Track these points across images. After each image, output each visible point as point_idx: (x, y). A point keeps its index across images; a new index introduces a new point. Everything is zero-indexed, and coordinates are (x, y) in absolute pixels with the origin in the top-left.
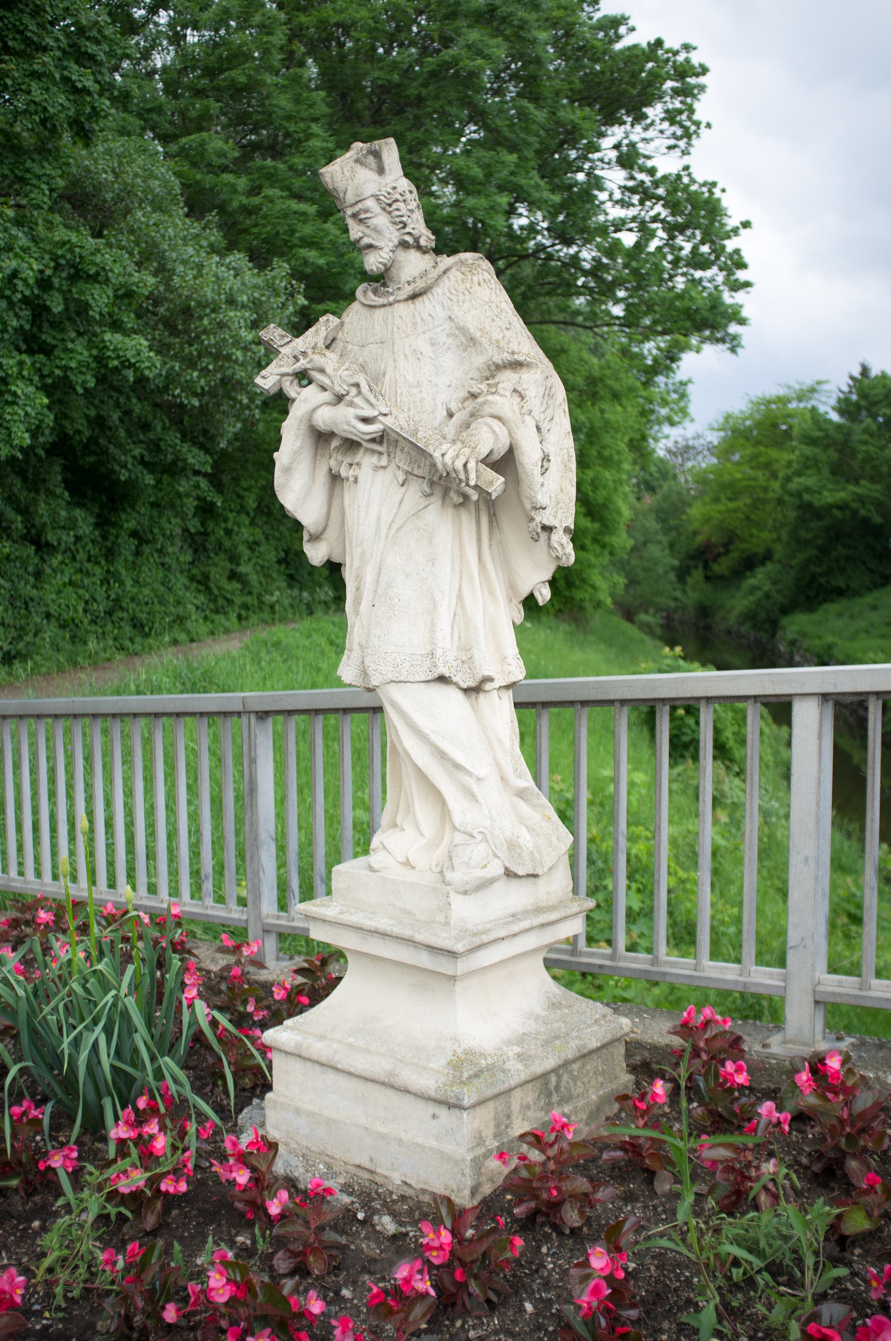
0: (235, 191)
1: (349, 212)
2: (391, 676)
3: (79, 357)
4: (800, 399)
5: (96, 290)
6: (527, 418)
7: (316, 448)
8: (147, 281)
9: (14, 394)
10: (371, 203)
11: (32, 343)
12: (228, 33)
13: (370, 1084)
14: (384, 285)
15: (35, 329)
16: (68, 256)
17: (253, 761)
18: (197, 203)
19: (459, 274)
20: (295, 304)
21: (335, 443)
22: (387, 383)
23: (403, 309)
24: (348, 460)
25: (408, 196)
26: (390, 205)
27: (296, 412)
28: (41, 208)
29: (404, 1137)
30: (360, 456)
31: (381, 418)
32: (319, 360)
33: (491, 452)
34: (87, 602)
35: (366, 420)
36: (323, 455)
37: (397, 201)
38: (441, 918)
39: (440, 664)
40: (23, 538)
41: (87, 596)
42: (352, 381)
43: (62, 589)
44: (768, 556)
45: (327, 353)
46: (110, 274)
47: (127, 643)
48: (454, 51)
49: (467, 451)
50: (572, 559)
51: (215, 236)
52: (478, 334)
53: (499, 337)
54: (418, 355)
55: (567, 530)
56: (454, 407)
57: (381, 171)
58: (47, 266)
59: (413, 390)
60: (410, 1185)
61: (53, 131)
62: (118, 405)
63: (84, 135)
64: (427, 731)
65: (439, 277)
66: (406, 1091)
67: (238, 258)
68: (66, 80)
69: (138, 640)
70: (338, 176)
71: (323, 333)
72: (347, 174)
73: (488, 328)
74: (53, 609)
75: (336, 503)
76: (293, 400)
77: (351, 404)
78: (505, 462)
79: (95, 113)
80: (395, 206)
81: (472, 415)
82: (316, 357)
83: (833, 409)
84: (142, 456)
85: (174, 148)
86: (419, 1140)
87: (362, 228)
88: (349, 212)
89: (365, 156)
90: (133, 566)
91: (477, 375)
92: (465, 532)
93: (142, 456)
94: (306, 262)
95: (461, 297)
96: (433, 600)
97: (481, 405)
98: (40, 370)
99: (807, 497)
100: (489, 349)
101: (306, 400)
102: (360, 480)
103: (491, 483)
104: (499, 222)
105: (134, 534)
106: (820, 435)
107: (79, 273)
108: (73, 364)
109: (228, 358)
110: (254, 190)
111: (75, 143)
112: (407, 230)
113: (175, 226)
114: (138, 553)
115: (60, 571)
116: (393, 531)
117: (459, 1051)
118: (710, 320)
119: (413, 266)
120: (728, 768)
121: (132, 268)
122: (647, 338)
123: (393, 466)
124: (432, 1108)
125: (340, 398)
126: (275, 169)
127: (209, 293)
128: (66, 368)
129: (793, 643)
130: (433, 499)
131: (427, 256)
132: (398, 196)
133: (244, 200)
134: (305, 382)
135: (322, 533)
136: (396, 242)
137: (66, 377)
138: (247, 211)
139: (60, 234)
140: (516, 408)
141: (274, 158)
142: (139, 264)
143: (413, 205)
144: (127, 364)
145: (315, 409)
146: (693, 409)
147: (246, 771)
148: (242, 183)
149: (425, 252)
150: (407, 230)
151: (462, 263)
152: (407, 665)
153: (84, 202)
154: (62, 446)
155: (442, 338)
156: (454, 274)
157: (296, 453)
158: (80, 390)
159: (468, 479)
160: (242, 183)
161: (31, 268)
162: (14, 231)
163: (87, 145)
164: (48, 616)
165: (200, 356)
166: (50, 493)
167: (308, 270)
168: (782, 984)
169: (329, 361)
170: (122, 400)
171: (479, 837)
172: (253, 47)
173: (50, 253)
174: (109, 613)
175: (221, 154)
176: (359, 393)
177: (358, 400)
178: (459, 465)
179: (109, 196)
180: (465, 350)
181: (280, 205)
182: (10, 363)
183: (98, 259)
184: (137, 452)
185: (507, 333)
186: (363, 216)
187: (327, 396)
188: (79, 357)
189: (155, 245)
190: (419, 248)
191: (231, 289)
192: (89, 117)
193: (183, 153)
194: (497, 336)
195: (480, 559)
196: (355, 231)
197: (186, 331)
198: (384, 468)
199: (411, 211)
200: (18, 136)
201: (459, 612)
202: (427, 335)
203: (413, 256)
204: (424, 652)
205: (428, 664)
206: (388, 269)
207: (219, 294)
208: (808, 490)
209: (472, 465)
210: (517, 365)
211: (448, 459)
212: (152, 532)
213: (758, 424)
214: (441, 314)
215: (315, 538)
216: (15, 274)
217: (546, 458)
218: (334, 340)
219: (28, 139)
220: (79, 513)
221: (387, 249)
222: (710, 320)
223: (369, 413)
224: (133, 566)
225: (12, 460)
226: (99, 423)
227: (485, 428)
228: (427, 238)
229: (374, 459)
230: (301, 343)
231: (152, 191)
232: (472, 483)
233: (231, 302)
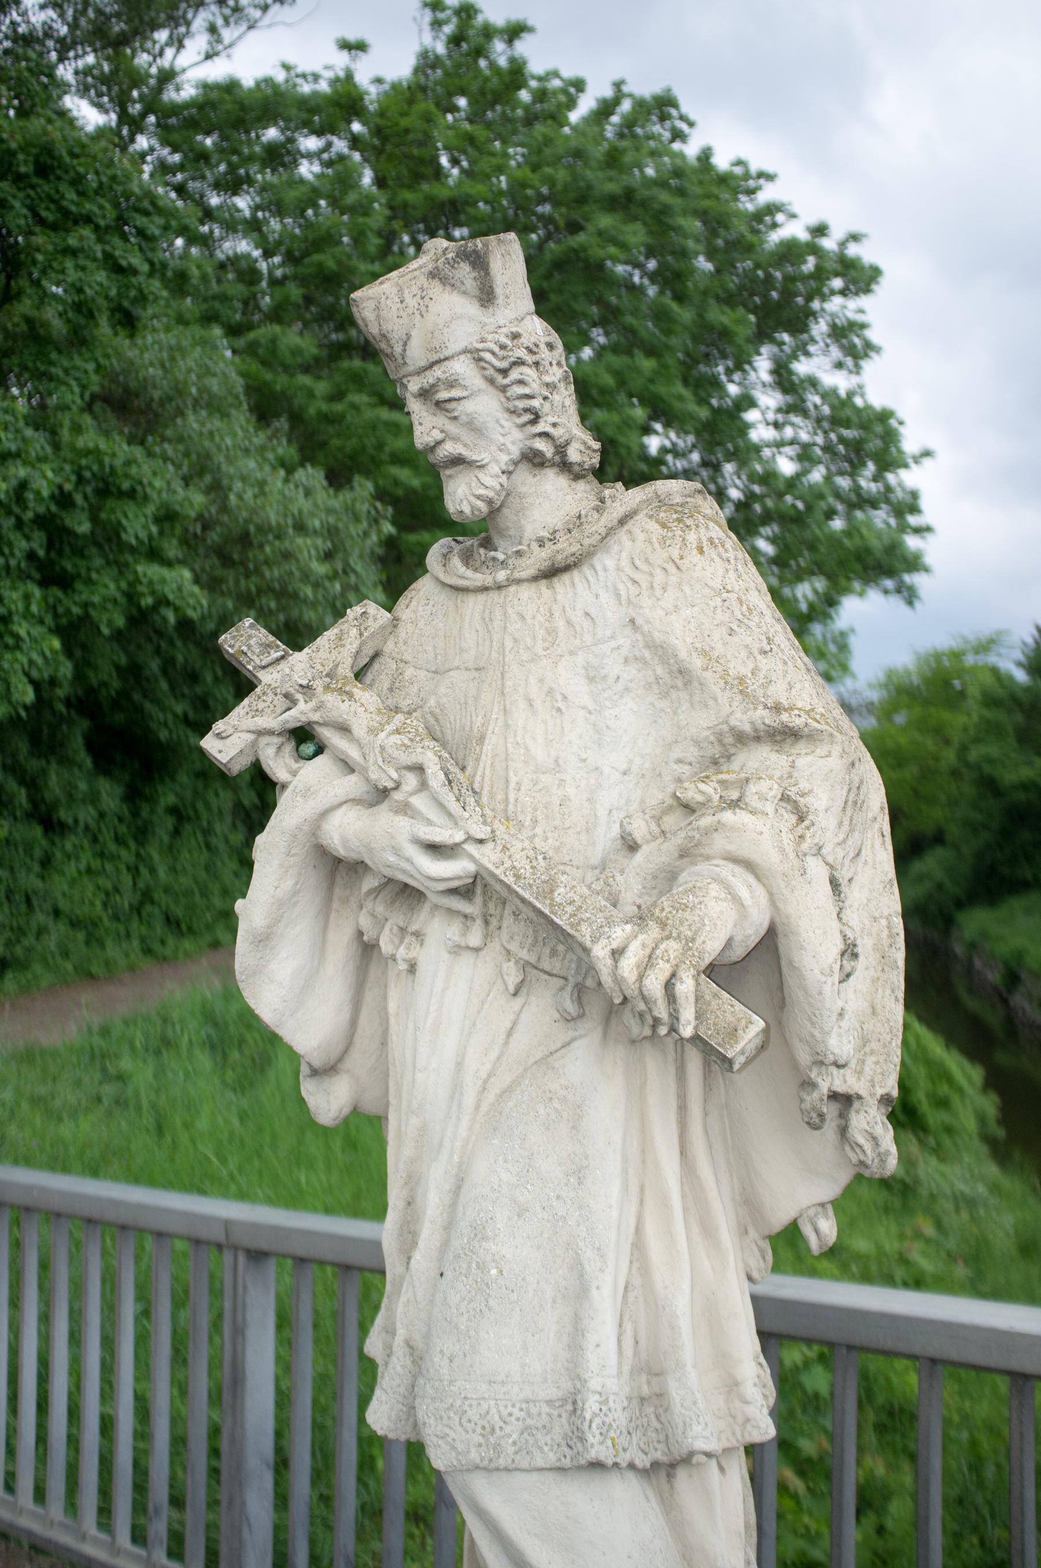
0: (311, 394)
1: (414, 385)
3: (103, 591)
4: (977, 652)
5: (131, 508)
6: (812, 862)
7: (329, 899)
8: (195, 500)
9: (17, 637)
10: (462, 367)
11: (52, 576)
12: (316, 214)
14: (487, 543)
15: (53, 555)
16: (95, 468)
17: (239, 1332)
18: (265, 406)
19: (653, 526)
20: (379, 531)
21: (369, 883)
22: (486, 759)
23: (528, 598)
24: (397, 919)
25: (545, 354)
26: (504, 372)
27: (288, 816)
28: (68, 408)
30: (425, 920)
32: (337, 706)
33: (729, 944)
34: (107, 894)
35: (434, 848)
36: (345, 901)
37: (519, 363)
39: (593, 1438)
40: (29, 815)
41: (109, 886)
42: (406, 759)
43: (75, 882)
44: (939, 838)
45: (357, 691)
46: (148, 490)
47: (156, 946)
48: (581, 238)
49: (673, 947)
50: (892, 1163)
51: (285, 449)
52: (697, 663)
53: (746, 671)
54: (557, 701)
55: (885, 1100)
56: (639, 829)
57: (487, 296)
58: (68, 480)
59: (546, 779)
61: (91, 315)
62: (158, 651)
63: (127, 321)
65: (610, 532)
67: (312, 476)
68: (108, 256)
69: (171, 941)
70: (392, 308)
71: (352, 643)
72: (412, 302)
73: (719, 649)
74: (63, 905)
75: (370, 998)
76: (284, 786)
77: (405, 809)
78: (758, 967)
79: (142, 298)
80: (514, 374)
81: (684, 853)
82: (331, 699)
83: (1019, 664)
84: (185, 715)
85: (241, 342)
87: (441, 420)
89: (452, 264)
90: (171, 850)
91: (692, 753)
92: (653, 1100)
93: (185, 715)
94: (396, 482)
95: (659, 577)
96: (578, 1268)
97: (707, 832)
98: (54, 608)
99: (987, 769)
100: (723, 698)
101: (307, 792)
102: (422, 969)
103: (733, 1033)
104: (631, 439)
105: (173, 811)
106: (1001, 697)
107: (108, 488)
108: (96, 599)
109: (295, 596)
110: (337, 396)
111: (116, 334)
112: (541, 427)
113: (234, 435)
114: (176, 833)
115: (76, 855)
116: (491, 1097)
118: (886, 565)
119: (551, 503)
120: (922, 1142)
121: (178, 485)
122: (799, 579)
123: (495, 946)
125: (382, 794)
126: (365, 371)
127: (273, 517)
128: (86, 605)
129: (972, 946)
130: (584, 1026)
131: (581, 486)
132: (522, 353)
133: (324, 407)
134: (309, 748)
135: (341, 1059)
136: (515, 452)
137: (87, 616)
138: (328, 419)
139: (90, 438)
140: (787, 838)
141: (364, 359)
142: (187, 481)
143: (555, 374)
144: (163, 601)
145: (325, 814)
146: (857, 663)
147: (228, 1346)
148: (322, 387)
149: (577, 477)
150: (541, 427)
151: (661, 502)
152: (513, 1429)
153: (128, 405)
154: (86, 702)
155: (614, 667)
156: (645, 526)
157: (283, 906)
158: (106, 631)
159: (675, 1016)
160: (322, 387)
161: (44, 481)
162: (29, 432)
163: (132, 336)
164: (57, 913)
165: (259, 592)
166: (66, 762)
167: (400, 492)
169: (361, 708)
170: (163, 645)
172: (344, 231)
173: (72, 463)
174: (137, 909)
175: (296, 352)
176: (424, 785)
177: (419, 802)
178: (654, 984)
179: (156, 394)
180: (665, 695)
181: (368, 414)
182: (14, 597)
183: (134, 470)
184: (179, 708)
185: (763, 662)
186: (443, 395)
187: (350, 785)
188: (103, 591)
189: (208, 456)
190: (565, 466)
191: (300, 512)
192: (135, 301)
193: (252, 349)
194: (740, 667)
195: (683, 1153)
196: (426, 427)
197: (243, 563)
198: (477, 950)
199: (551, 386)
200: (46, 325)
201: (637, 1281)
202: (580, 659)
203: (553, 482)
204: (553, 1393)
205: (561, 1427)
206: (495, 511)
207: (286, 516)
208: (990, 761)
209: (686, 987)
210: (784, 736)
211: (628, 966)
212: (194, 807)
213: (928, 681)
214: (612, 613)
215: (325, 1071)
216: (23, 485)
217: (850, 951)
218: (376, 655)
219: (58, 326)
220: (104, 785)
221: (495, 469)
222: (886, 565)
224: (171, 850)
225: (14, 721)
226: (133, 672)
227: (714, 890)
228: (583, 448)
229: (453, 931)
230: (300, 664)
231: (208, 391)
232: (687, 1032)
233: (300, 528)
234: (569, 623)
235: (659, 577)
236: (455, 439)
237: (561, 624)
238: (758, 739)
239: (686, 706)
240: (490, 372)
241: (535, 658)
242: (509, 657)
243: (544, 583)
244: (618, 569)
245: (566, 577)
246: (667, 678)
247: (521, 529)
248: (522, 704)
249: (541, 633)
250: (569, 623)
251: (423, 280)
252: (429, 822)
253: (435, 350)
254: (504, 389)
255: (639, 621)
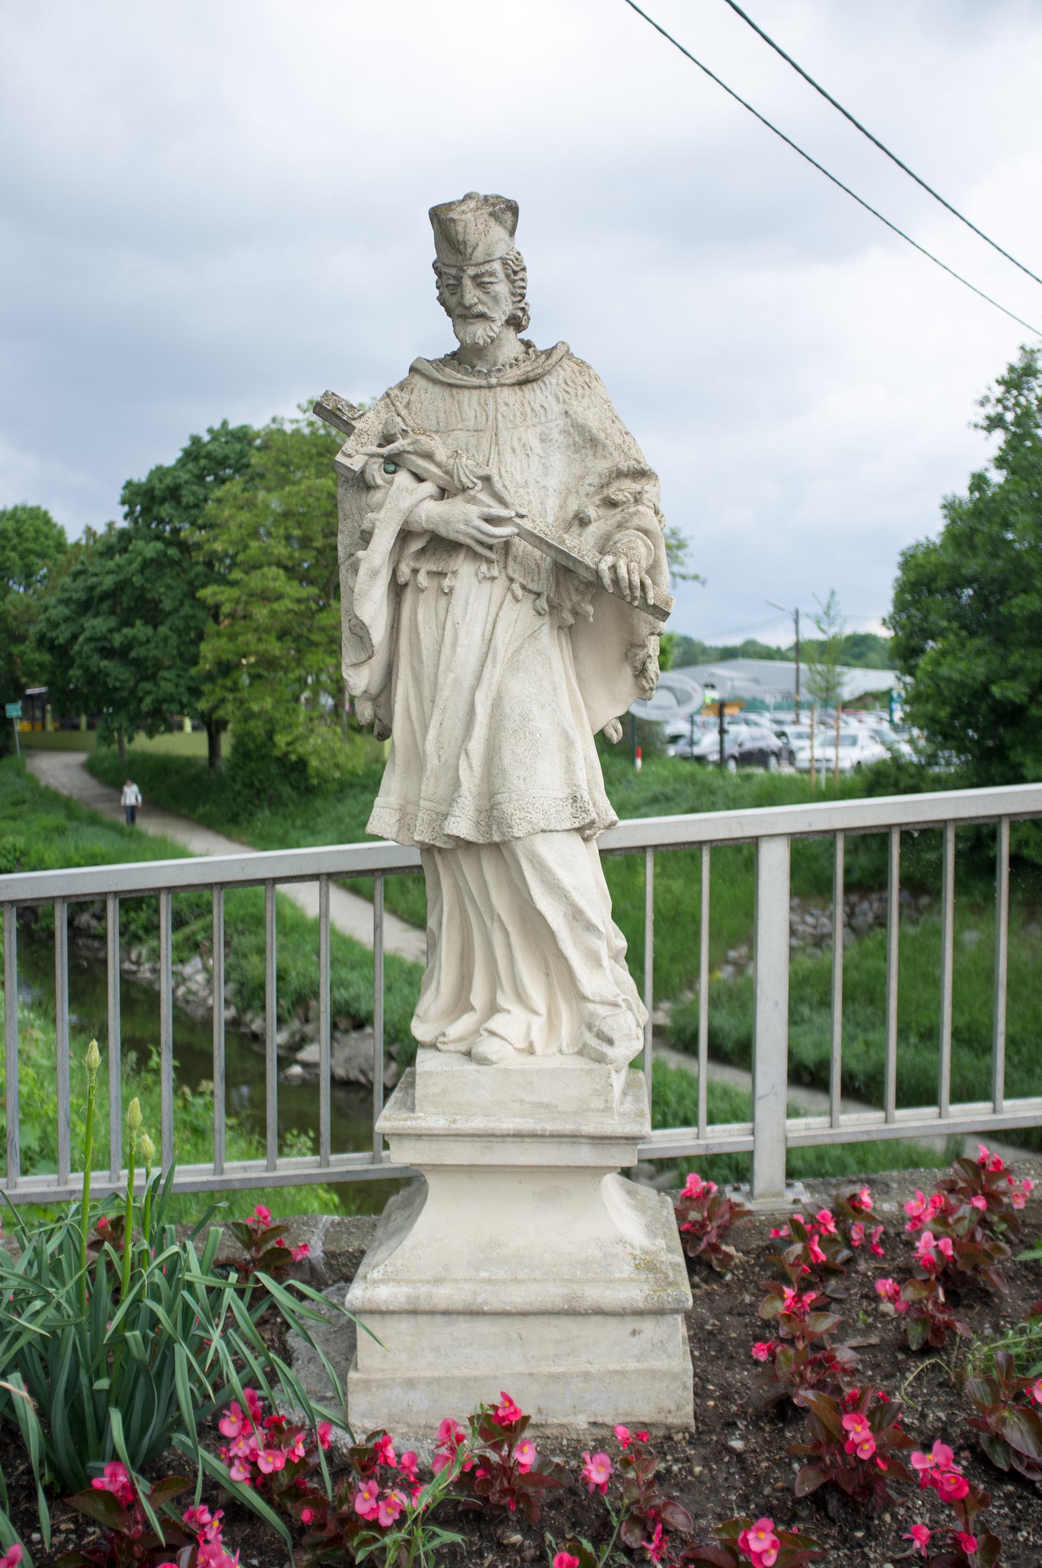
2: (543, 825)
13: (530, 1320)
26: (515, 273)
29: (593, 1369)
31: (517, 520)
35: (490, 520)
38: (599, 1103)
59: (521, 491)
60: (603, 1425)
64: (569, 888)
66: (601, 1312)
72: (481, 227)
77: (473, 500)
86: (612, 1367)
87: (478, 292)
88: (471, 271)
95: (580, 391)
100: (616, 454)
117: (638, 1252)
124: (630, 1324)
155: (555, 435)
168: (751, 1138)
171: (623, 1005)
180: (577, 451)
186: (486, 279)
202: (538, 429)
214: (556, 408)
223: (498, 510)
234: (532, 410)
235: (580, 391)
236: (484, 304)
237: (528, 410)
238: (626, 476)
239: (590, 457)
240: (510, 272)
241: (516, 427)
242: (500, 425)
243: (517, 388)
244: (558, 384)
245: (529, 386)
246: (581, 443)
247: (496, 357)
248: (509, 451)
249: (518, 414)
250: (532, 410)
251: (486, 216)
252: (489, 506)
253: (489, 255)
254: (513, 282)
255: (571, 412)
